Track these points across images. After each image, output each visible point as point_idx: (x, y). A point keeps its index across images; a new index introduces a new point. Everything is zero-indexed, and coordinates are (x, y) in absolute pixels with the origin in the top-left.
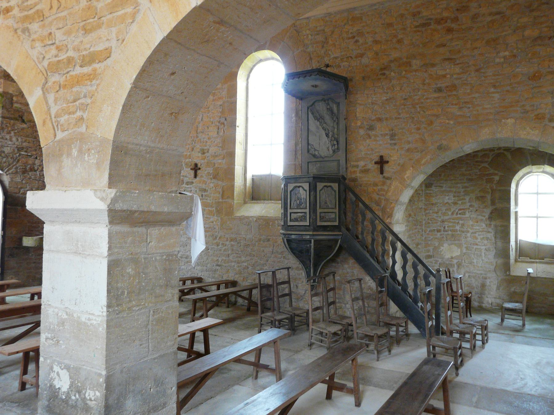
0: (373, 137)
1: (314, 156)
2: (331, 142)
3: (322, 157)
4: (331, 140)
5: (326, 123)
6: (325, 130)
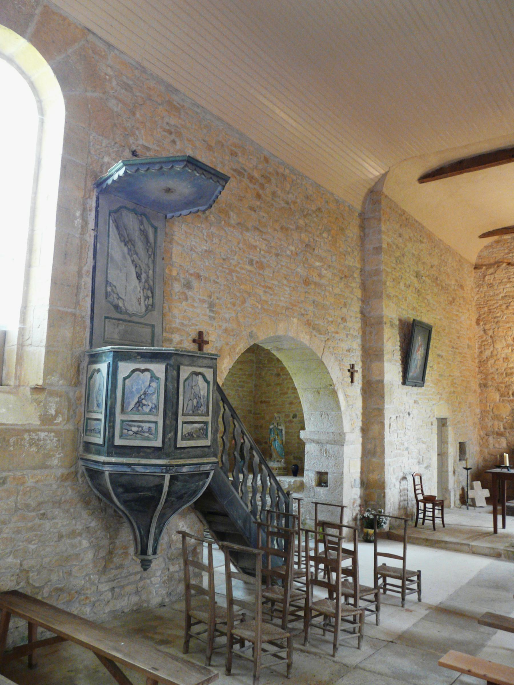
0: (190, 301)
1: (117, 307)
2: (143, 290)
3: (128, 314)
4: (144, 288)
5: (137, 254)
6: (136, 267)
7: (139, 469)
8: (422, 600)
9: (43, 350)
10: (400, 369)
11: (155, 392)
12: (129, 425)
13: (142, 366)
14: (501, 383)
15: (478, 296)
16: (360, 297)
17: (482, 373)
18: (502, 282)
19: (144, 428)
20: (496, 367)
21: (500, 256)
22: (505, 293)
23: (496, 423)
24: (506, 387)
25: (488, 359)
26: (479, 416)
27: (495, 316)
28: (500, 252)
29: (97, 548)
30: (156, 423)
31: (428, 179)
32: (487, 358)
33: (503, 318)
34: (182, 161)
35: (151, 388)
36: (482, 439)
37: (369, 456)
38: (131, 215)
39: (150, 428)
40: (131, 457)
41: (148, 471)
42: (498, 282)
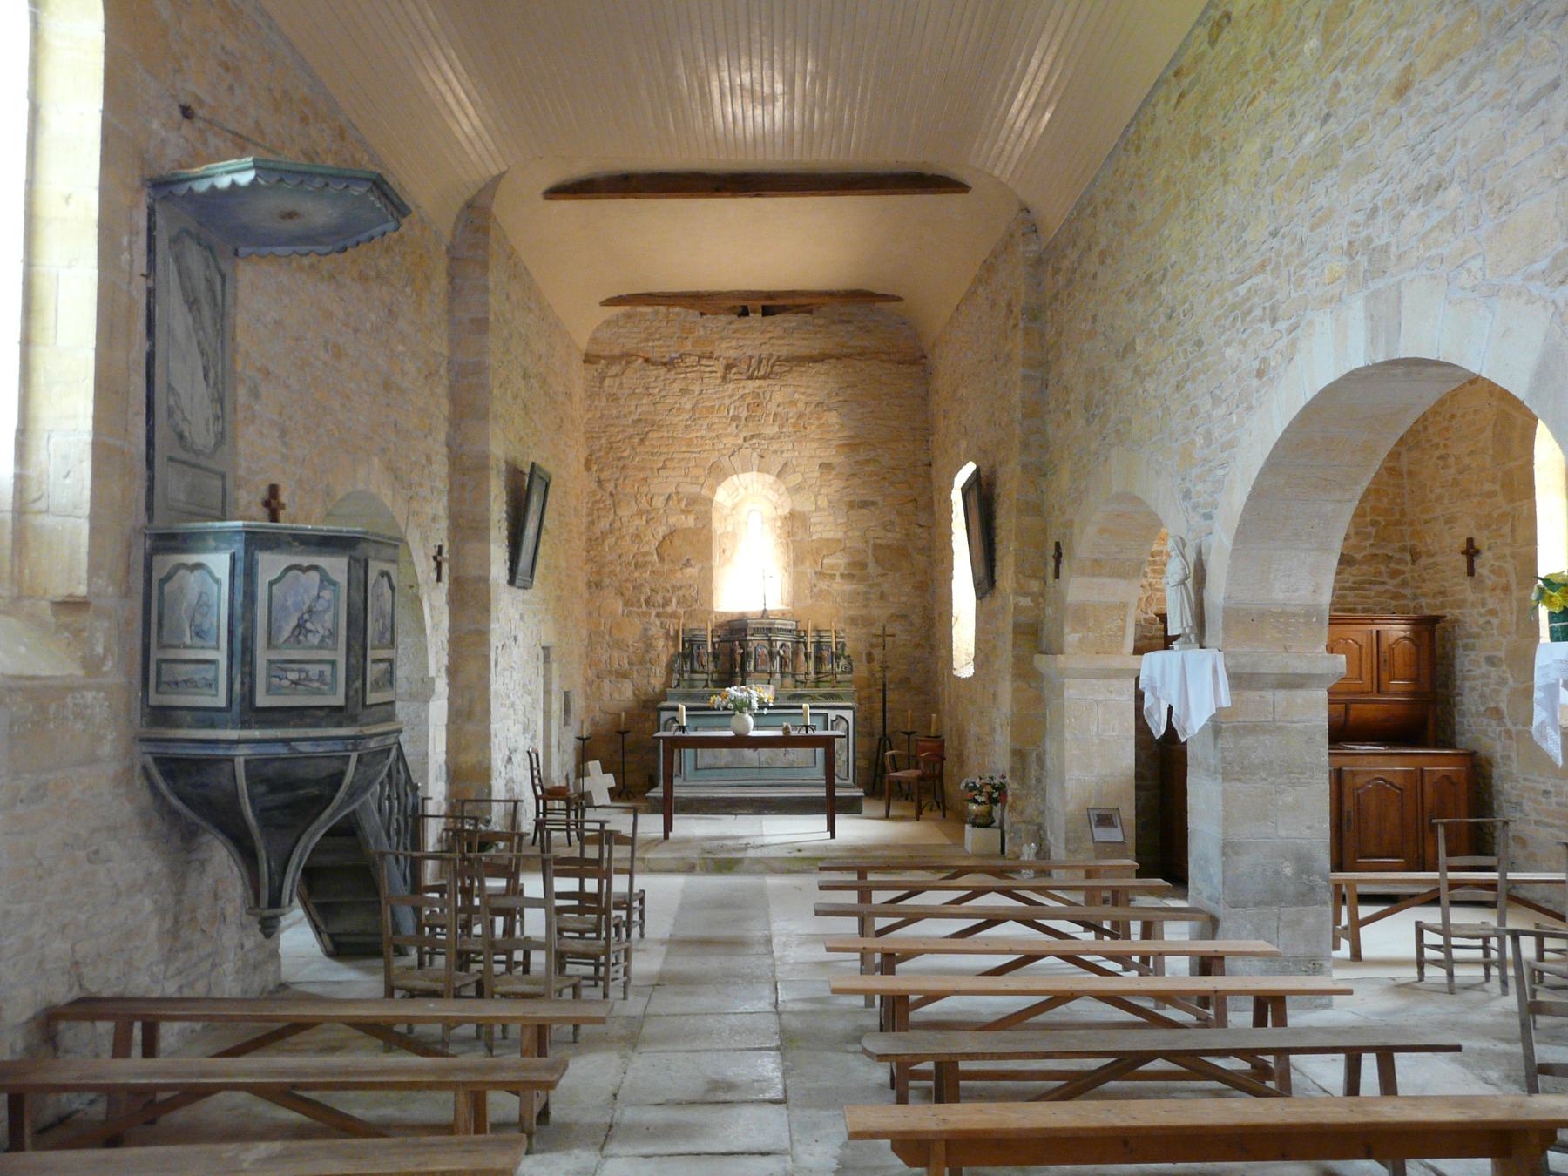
7: (305, 748)
8: (646, 936)
9: (84, 527)
10: (507, 556)
11: (329, 607)
12: (282, 669)
13: (305, 561)
14: (626, 581)
15: (589, 415)
16: (447, 413)
17: (592, 560)
18: (634, 393)
19: (310, 673)
20: (619, 551)
21: (630, 344)
22: (640, 415)
23: (615, 654)
24: (634, 588)
25: (604, 535)
26: (586, 643)
27: (619, 455)
28: (633, 335)
29: (161, 911)
30: (333, 663)
31: (563, 195)
32: (602, 533)
33: (633, 459)
34: (367, 180)
35: (321, 601)
36: (590, 684)
37: (459, 722)
38: (195, 247)
39: (321, 673)
40: (289, 727)
41: (322, 749)
42: (627, 392)
